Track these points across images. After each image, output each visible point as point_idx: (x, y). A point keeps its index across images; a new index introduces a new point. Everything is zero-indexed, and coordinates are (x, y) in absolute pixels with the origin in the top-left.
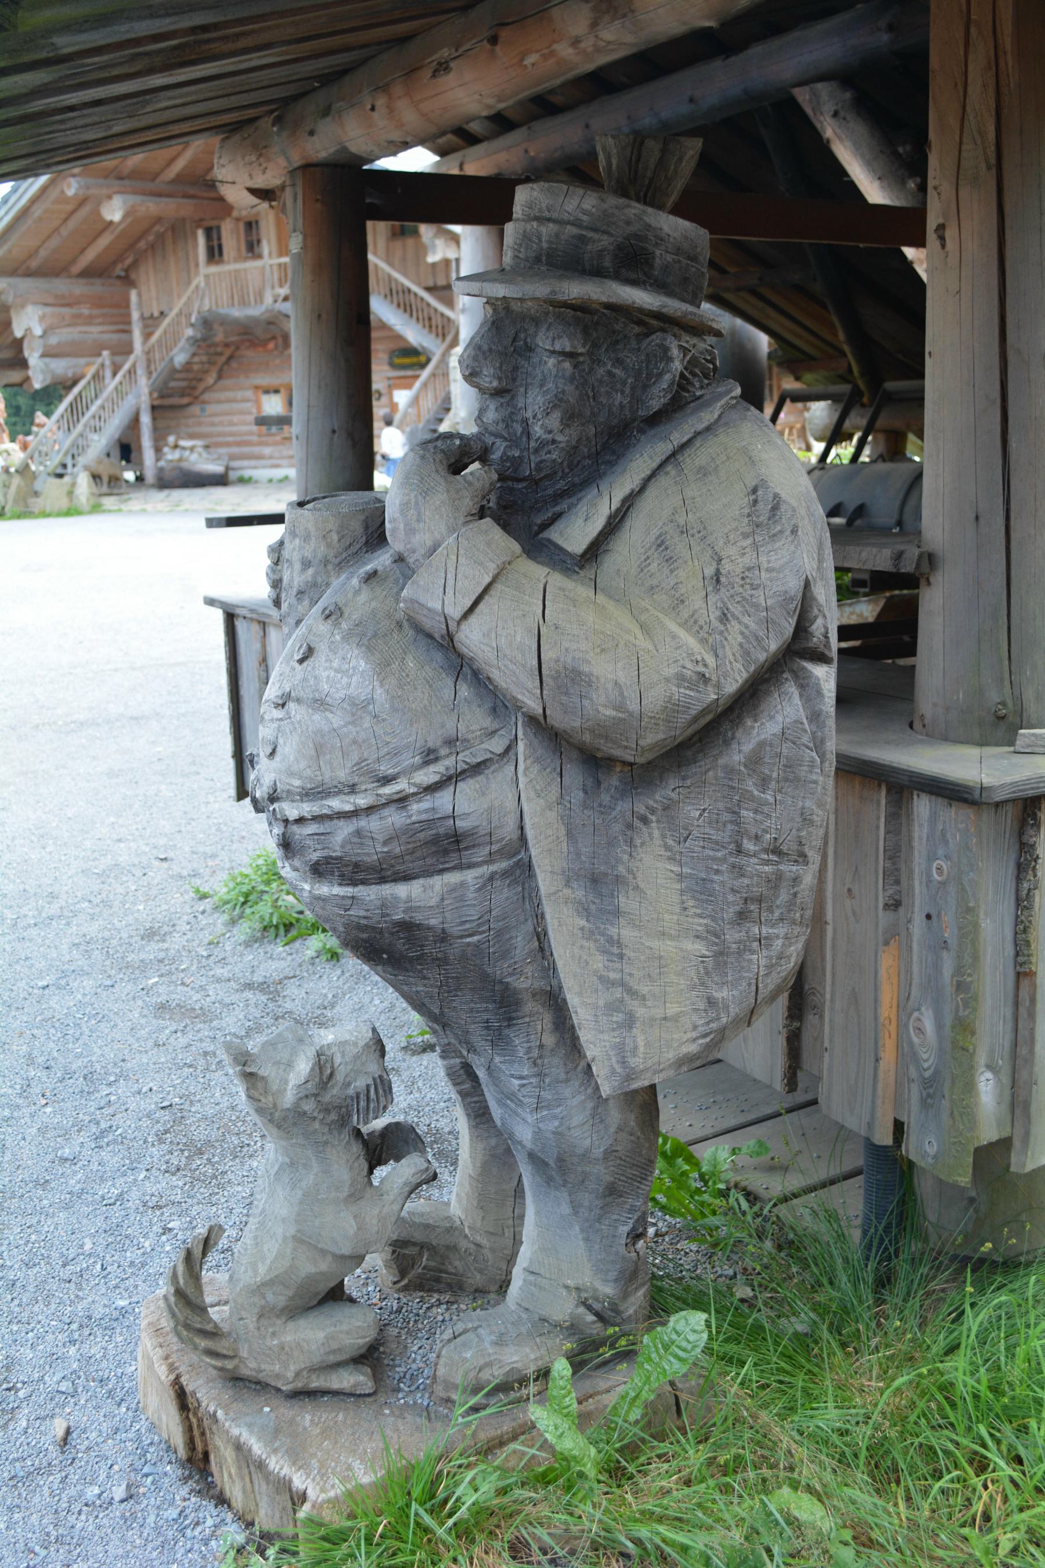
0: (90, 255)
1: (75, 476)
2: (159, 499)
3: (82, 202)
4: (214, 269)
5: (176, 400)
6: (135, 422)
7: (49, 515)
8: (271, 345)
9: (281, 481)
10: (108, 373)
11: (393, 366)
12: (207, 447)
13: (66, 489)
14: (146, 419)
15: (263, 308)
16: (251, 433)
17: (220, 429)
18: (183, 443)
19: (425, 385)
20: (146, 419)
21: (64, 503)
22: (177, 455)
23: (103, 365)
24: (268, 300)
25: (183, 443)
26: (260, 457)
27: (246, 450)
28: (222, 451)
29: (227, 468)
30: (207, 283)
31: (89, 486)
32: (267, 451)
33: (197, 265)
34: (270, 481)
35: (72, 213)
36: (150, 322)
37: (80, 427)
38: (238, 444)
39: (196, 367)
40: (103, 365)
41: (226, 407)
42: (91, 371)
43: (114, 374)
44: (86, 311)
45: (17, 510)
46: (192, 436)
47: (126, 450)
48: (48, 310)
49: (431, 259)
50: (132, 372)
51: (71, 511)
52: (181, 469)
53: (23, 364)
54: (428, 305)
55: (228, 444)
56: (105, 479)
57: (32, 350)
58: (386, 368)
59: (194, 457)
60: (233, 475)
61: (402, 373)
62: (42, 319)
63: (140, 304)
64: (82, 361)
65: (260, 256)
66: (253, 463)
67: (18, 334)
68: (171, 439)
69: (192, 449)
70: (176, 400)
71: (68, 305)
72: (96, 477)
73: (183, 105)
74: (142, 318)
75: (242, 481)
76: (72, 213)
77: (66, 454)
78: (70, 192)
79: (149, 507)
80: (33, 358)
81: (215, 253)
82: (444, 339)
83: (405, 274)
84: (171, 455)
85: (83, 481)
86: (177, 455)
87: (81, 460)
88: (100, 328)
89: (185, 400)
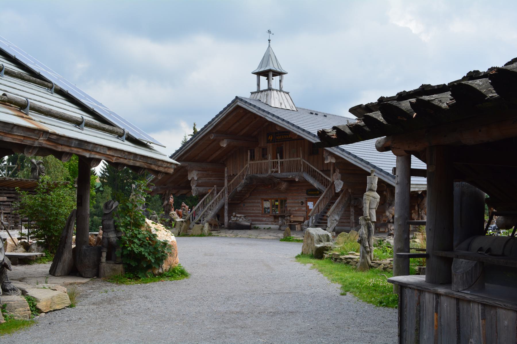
0: (214, 156)
1: (204, 224)
2: (230, 233)
3: (214, 141)
4: (252, 162)
5: (236, 202)
6: (223, 208)
7: (194, 236)
8: (270, 186)
9: (268, 229)
10: (215, 192)
11: (307, 194)
12: (245, 217)
13: (200, 228)
14: (226, 207)
15: (268, 175)
16: (259, 213)
17: (249, 211)
18: (237, 215)
19: (321, 201)
20: (226, 207)
21: (200, 232)
22: (235, 219)
23: (214, 190)
24: (270, 172)
25: (237, 215)
26: (262, 221)
27: (257, 218)
28: (249, 218)
29: (251, 224)
30: (250, 166)
31: (208, 227)
32: (264, 219)
33: (247, 160)
34: (265, 229)
35: (211, 143)
36: (230, 178)
37: (206, 209)
38: (255, 216)
39: (243, 192)
40: (214, 190)
41: (252, 204)
42: (210, 191)
43: (217, 193)
44: (210, 173)
45: (184, 233)
46: (239, 213)
47: (219, 215)
48: (200, 172)
49: (326, 162)
50: (223, 192)
51: (202, 235)
52: (236, 223)
53: (190, 188)
54: (322, 176)
55: (251, 216)
56: (213, 225)
57: (193, 184)
58: (305, 195)
59: (241, 220)
60: (253, 226)
61: (311, 197)
62: (197, 175)
63: (227, 172)
64: (208, 188)
65: (267, 159)
66: (259, 223)
67: (189, 179)
68: (234, 214)
69: (240, 217)
70: (236, 202)
71: (205, 171)
72: (210, 225)
73: (69, 111)
74: (228, 176)
75: (256, 228)
76: (211, 143)
77: (201, 217)
78: (212, 138)
79: (227, 235)
80: (193, 187)
81: (252, 158)
82: (326, 187)
83: (313, 166)
84: (234, 219)
85: (206, 226)
86: (235, 219)
87: (206, 219)
88: (214, 179)
89: (239, 202)
